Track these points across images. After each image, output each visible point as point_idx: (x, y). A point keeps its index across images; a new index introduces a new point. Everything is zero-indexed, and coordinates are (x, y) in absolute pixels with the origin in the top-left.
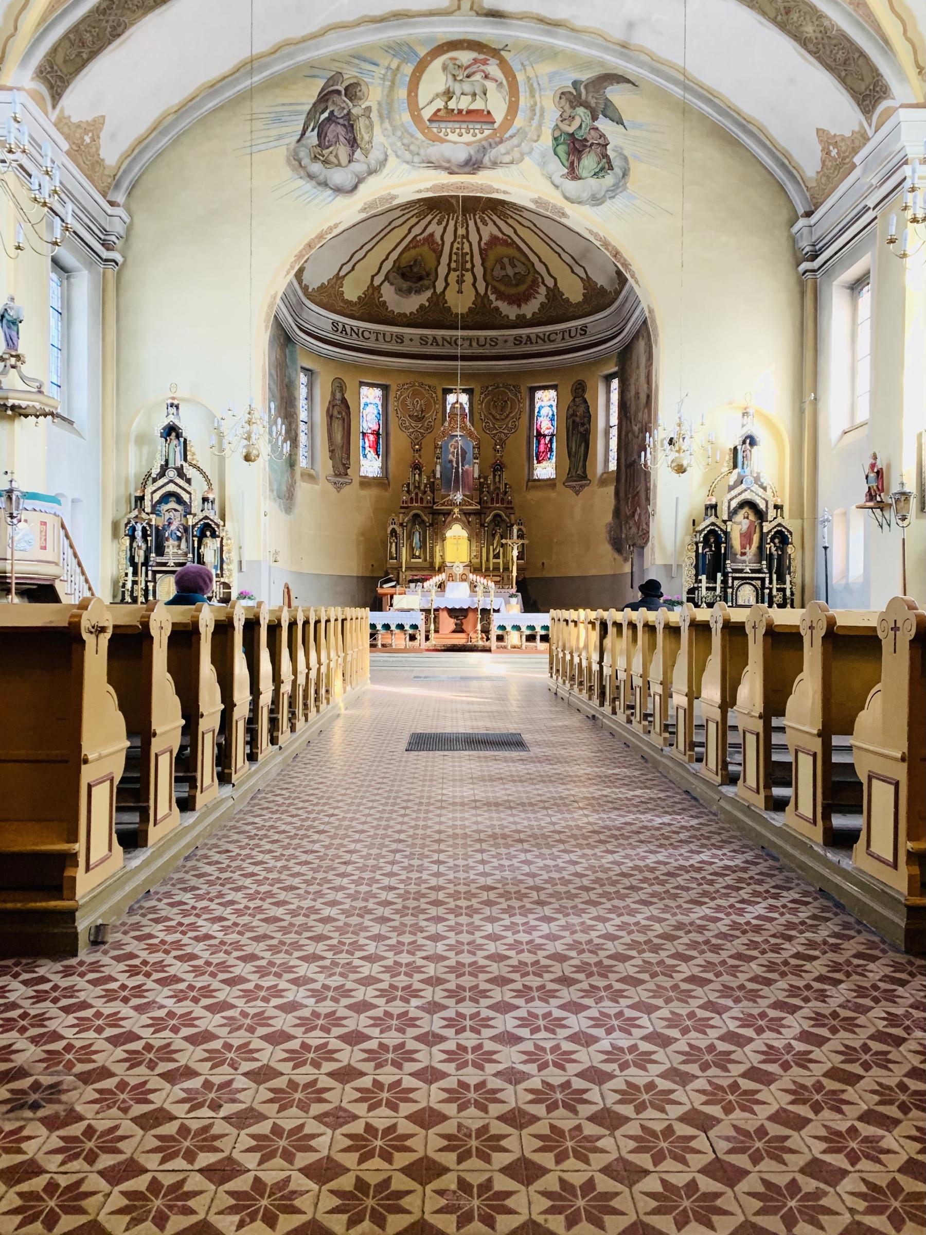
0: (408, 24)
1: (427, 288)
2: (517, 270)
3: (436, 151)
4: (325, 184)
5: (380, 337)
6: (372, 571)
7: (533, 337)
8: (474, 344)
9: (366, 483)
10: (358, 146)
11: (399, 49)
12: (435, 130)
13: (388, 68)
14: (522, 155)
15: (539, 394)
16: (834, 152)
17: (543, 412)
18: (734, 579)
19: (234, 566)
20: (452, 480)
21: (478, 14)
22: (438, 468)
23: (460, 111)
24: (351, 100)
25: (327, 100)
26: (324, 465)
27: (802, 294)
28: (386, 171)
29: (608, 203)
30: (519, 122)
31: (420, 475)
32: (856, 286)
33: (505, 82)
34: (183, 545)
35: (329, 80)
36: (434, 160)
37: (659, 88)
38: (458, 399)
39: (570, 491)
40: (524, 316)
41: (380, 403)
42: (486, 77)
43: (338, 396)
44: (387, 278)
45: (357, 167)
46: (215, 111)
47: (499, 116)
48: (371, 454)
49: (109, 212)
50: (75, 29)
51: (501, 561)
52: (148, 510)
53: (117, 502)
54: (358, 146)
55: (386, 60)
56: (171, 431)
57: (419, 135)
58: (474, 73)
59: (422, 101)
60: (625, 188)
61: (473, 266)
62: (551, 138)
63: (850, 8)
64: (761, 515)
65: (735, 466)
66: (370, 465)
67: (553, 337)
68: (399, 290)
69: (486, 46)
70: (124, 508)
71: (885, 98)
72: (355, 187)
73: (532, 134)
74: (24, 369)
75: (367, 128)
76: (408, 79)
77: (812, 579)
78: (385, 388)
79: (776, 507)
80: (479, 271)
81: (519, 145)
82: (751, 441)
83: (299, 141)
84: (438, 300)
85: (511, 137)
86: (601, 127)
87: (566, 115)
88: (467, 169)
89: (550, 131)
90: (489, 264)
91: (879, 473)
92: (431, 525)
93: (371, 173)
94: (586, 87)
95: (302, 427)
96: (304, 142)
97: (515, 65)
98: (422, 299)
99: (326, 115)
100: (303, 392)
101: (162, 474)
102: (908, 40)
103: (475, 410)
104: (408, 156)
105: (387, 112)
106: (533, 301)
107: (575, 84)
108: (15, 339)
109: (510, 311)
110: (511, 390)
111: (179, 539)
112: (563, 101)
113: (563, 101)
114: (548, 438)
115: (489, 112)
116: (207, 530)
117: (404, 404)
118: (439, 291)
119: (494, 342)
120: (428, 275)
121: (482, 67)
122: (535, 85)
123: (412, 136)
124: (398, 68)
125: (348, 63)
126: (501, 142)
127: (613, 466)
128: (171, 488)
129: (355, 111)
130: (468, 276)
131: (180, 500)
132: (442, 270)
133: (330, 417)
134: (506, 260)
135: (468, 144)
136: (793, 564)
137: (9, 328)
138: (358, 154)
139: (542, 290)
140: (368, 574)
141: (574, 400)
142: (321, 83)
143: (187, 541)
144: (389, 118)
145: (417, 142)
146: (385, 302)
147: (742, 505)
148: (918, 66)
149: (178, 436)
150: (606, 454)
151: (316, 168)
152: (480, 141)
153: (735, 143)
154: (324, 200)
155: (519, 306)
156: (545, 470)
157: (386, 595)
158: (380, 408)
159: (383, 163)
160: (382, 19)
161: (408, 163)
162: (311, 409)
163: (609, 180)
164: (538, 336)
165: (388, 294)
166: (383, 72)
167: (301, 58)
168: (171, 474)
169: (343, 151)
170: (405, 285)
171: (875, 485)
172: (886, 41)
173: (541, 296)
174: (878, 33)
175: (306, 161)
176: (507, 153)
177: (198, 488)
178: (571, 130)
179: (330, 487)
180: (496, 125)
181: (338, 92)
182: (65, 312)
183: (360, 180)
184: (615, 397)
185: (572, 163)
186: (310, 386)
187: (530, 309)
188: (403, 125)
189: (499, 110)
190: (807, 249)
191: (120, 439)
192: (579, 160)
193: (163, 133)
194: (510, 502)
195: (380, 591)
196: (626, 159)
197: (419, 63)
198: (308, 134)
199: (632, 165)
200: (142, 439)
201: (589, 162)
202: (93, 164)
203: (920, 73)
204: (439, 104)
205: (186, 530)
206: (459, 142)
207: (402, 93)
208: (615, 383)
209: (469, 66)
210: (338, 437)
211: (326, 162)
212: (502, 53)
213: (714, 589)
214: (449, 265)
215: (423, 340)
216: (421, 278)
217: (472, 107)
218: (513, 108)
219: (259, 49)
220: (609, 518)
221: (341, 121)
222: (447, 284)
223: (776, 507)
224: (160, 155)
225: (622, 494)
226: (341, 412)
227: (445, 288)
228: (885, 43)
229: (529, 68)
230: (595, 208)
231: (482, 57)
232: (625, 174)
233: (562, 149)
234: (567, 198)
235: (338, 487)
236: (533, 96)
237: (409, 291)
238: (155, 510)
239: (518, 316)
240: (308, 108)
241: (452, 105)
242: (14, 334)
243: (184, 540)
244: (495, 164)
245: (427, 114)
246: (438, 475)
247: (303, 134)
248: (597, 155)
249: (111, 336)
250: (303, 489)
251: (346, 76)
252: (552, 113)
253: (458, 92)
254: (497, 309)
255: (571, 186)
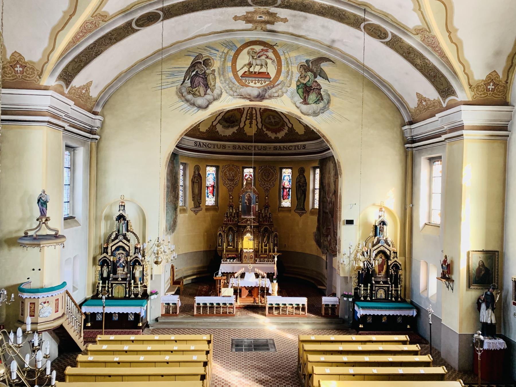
0: (233, 34)
1: (236, 126)
2: (276, 120)
3: (245, 90)
4: (193, 104)
5: (216, 146)
6: (210, 248)
7: (282, 147)
8: (256, 149)
9: (208, 208)
10: (209, 87)
11: (228, 45)
12: (244, 81)
13: (223, 52)
14: (283, 93)
15: (284, 170)
16: (424, 103)
17: (286, 178)
18: (376, 287)
19: (149, 277)
20: (247, 210)
21: (264, 31)
22: (240, 206)
23: (255, 73)
24: (206, 66)
25: (195, 66)
26: (190, 203)
27: (406, 156)
28: (221, 99)
29: (321, 115)
30: (281, 78)
31: (232, 210)
32: (432, 160)
33: (275, 60)
34: (126, 270)
35: (196, 57)
36: (243, 95)
37: (344, 64)
38: (248, 172)
39: (297, 214)
40: (278, 137)
41: (215, 173)
42: (267, 57)
43: (197, 173)
44: (219, 122)
45: (208, 97)
46: (143, 70)
47: (273, 75)
48: (211, 196)
49: (94, 118)
50: (78, 56)
51: (267, 248)
52: (110, 254)
53: (95, 248)
54: (209, 87)
55: (222, 49)
56: (121, 217)
57: (236, 83)
58: (262, 55)
59: (238, 68)
60: (328, 109)
61: (257, 118)
62: (295, 86)
63: (439, 58)
64: (388, 257)
65: (376, 235)
66: (210, 201)
67: (290, 148)
68: (224, 127)
69: (268, 44)
70: (98, 251)
71: (453, 95)
72: (207, 106)
73: (287, 84)
74: (49, 223)
75: (213, 79)
76: (232, 57)
77: (410, 286)
78: (217, 167)
79: (394, 253)
80: (259, 120)
81: (281, 89)
82: (383, 223)
83: (182, 84)
84: (241, 131)
85: (278, 85)
86: (318, 81)
87: (303, 75)
88: (258, 99)
89: (295, 82)
90: (263, 118)
91: (448, 266)
92: (237, 232)
93: (215, 100)
94: (311, 63)
95: (181, 188)
96: (184, 85)
97: (280, 53)
98: (235, 129)
99: (194, 73)
100: (181, 172)
101: (116, 238)
102: (466, 74)
103: (256, 177)
104: (231, 93)
105: (222, 73)
106: (283, 132)
107: (307, 61)
108: (45, 211)
109: (272, 135)
110: (272, 169)
111: (124, 267)
112: (302, 69)
113: (302, 69)
114: (288, 190)
115: (268, 73)
116: (136, 262)
117: (225, 174)
118: (241, 126)
119: (265, 148)
120: (237, 121)
121: (265, 53)
122: (289, 62)
123: (234, 84)
124: (227, 53)
125: (205, 50)
126: (274, 87)
127: (317, 206)
128: (120, 244)
129: (207, 71)
130: (254, 122)
131: (124, 249)
132: (243, 119)
133: (193, 182)
134: (271, 117)
135: (258, 88)
136: (401, 277)
137: (42, 206)
138: (209, 91)
139: (286, 128)
140: (208, 249)
141: (299, 175)
142: (192, 58)
143: (127, 268)
144: (223, 75)
145: (236, 86)
146: (218, 131)
147: (379, 253)
148: (469, 84)
149: (124, 219)
150: (314, 200)
151: (190, 97)
152: (264, 86)
153: (378, 89)
154: (193, 111)
155: (276, 133)
156: (286, 203)
157: (218, 280)
158: (215, 175)
159: (220, 95)
160: (221, 32)
161: (231, 96)
162: (184, 181)
163: (321, 105)
164: (284, 147)
165: (219, 128)
166: (221, 54)
167: (183, 48)
168: (121, 237)
169: (202, 90)
170: (227, 125)
171: (446, 271)
172: (455, 73)
173: (286, 130)
174: (451, 69)
175: (185, 94)
176: (276, 92)
177: (133, 242)
178: (305, 82)
179: (192, 213)
180: (271, 79)
181: (200, 63)
182: (72, 168)
183: (210, 103)
184: (318, 176)
185: (305, 97)
186: (184, 170)
187: (281, 135)
188: (229, 78)
189: (273, 74)
190: (409, 138)
191: (97, 220)
192: (308, 95)
193: (120, 81)
194: (271, 222)
195: (215, 278)
196: (329, 95)
197: (237, 50)
198: (186, 81)
199: (332, 98)
200: (107, 218)
201: (313, 97)
202: (86, 100)
203: (470, 88)
204: (246, 69)
205: (127, 262)
206: (254, 87)
207: (229, 64)
208: (318, 171)
209: (259, 53)
210: (196, 191)
211: (194, 94)
212: (275, 47)
213: (367, 290)
214: (246, 117)
215: (234, 147)
216: (234, 122)
217: (261, 71)
218: (279, 72)
219: (164, 46)
220: (315, 230)
221: (201, 76)
222: (245, 124)
223: (394, 253)
224: (117, 90)
225: (321, 221)
226: (198, 180)
227: (244, 126)
228: (455, 74)
229: (286, 54)
230: (315, 118)
231: (266, 48)
232: (329, 102)
233: (300, 91)
234: (302, 113)
235: (196, 212)
236: (288, 67)
237: (228, 127)
238: (113, 254)
239: (275, 138)
240: (187, 69)
241: (251, 70)
242: (44, 209)
243: (126, 268)
244: (270, 97)
245: (240, 73)
246: (240, 210)
247: (184, 82)
248: (316, 93)
249: (94, 173)
250: (181, 217)
251: (203, 56)
252: (296, 75)
253: (254, 64)
254: (266, 134)
255: (304, 107)
